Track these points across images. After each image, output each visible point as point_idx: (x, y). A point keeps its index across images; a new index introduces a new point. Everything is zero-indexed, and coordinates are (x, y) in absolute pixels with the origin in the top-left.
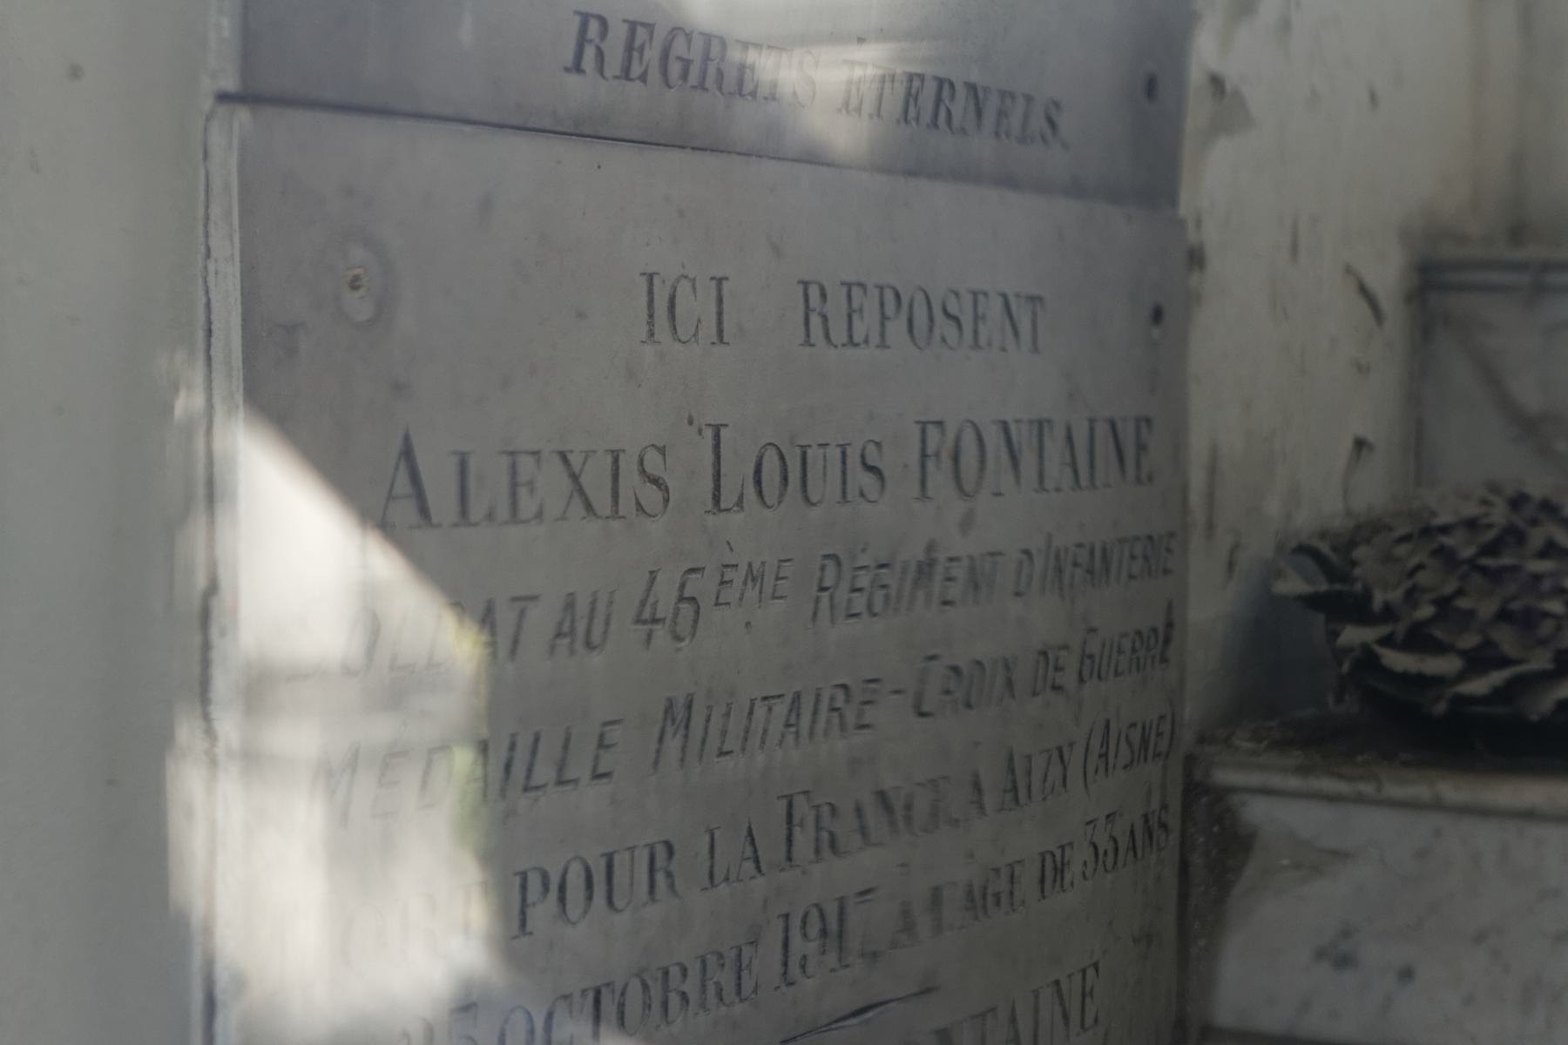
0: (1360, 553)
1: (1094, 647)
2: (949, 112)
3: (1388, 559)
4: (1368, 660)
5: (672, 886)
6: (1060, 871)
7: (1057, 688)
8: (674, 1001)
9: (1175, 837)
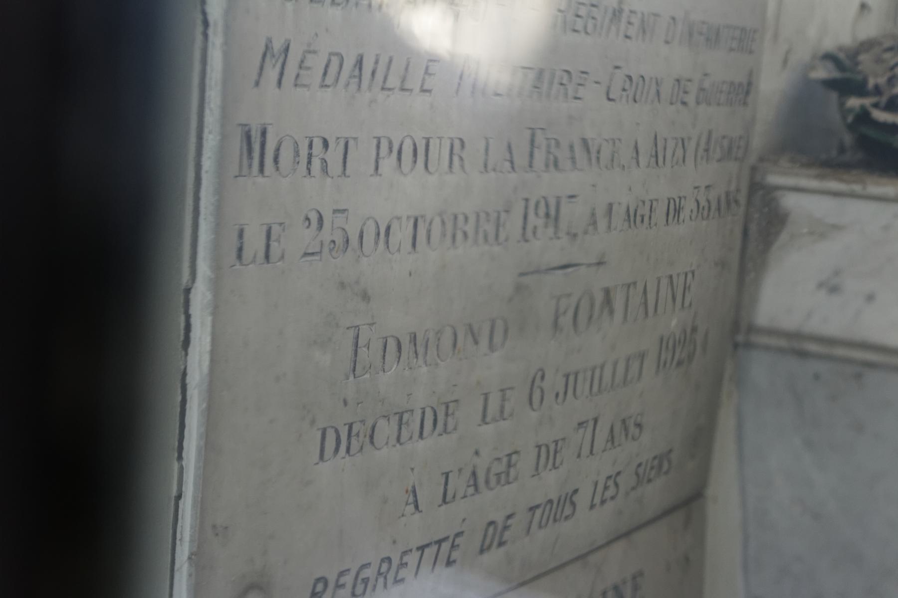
0: (862, 57)
1: (707, 84)
3: (879, 61)
4: (864, 117)
5: (462, 167)
6: (678, 211)
7: (684, 103)
8: (460, 236)
9: (742, 210)
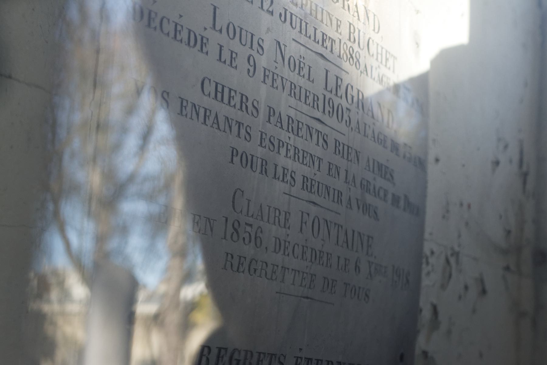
2: (292, 127)
